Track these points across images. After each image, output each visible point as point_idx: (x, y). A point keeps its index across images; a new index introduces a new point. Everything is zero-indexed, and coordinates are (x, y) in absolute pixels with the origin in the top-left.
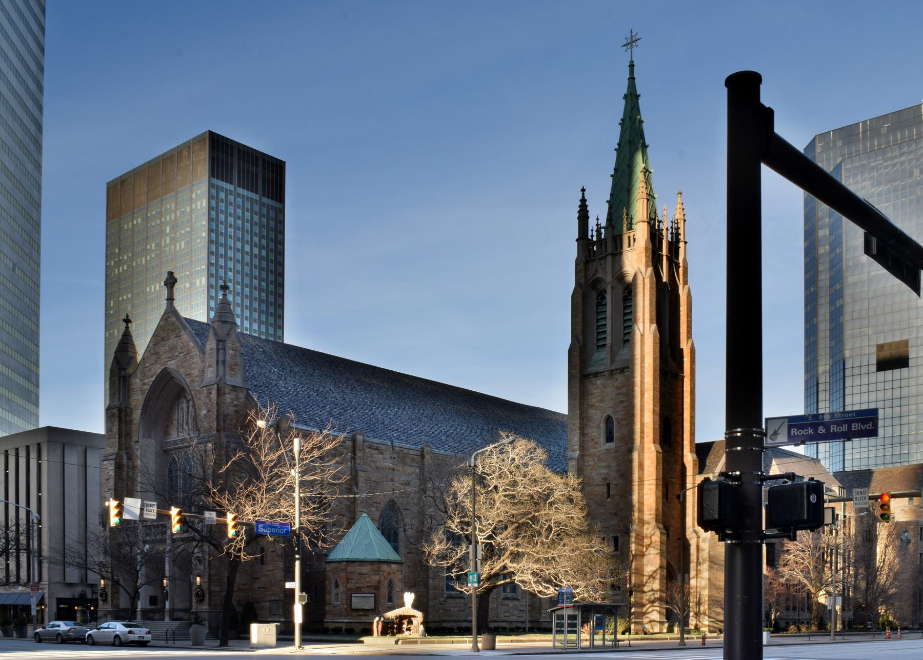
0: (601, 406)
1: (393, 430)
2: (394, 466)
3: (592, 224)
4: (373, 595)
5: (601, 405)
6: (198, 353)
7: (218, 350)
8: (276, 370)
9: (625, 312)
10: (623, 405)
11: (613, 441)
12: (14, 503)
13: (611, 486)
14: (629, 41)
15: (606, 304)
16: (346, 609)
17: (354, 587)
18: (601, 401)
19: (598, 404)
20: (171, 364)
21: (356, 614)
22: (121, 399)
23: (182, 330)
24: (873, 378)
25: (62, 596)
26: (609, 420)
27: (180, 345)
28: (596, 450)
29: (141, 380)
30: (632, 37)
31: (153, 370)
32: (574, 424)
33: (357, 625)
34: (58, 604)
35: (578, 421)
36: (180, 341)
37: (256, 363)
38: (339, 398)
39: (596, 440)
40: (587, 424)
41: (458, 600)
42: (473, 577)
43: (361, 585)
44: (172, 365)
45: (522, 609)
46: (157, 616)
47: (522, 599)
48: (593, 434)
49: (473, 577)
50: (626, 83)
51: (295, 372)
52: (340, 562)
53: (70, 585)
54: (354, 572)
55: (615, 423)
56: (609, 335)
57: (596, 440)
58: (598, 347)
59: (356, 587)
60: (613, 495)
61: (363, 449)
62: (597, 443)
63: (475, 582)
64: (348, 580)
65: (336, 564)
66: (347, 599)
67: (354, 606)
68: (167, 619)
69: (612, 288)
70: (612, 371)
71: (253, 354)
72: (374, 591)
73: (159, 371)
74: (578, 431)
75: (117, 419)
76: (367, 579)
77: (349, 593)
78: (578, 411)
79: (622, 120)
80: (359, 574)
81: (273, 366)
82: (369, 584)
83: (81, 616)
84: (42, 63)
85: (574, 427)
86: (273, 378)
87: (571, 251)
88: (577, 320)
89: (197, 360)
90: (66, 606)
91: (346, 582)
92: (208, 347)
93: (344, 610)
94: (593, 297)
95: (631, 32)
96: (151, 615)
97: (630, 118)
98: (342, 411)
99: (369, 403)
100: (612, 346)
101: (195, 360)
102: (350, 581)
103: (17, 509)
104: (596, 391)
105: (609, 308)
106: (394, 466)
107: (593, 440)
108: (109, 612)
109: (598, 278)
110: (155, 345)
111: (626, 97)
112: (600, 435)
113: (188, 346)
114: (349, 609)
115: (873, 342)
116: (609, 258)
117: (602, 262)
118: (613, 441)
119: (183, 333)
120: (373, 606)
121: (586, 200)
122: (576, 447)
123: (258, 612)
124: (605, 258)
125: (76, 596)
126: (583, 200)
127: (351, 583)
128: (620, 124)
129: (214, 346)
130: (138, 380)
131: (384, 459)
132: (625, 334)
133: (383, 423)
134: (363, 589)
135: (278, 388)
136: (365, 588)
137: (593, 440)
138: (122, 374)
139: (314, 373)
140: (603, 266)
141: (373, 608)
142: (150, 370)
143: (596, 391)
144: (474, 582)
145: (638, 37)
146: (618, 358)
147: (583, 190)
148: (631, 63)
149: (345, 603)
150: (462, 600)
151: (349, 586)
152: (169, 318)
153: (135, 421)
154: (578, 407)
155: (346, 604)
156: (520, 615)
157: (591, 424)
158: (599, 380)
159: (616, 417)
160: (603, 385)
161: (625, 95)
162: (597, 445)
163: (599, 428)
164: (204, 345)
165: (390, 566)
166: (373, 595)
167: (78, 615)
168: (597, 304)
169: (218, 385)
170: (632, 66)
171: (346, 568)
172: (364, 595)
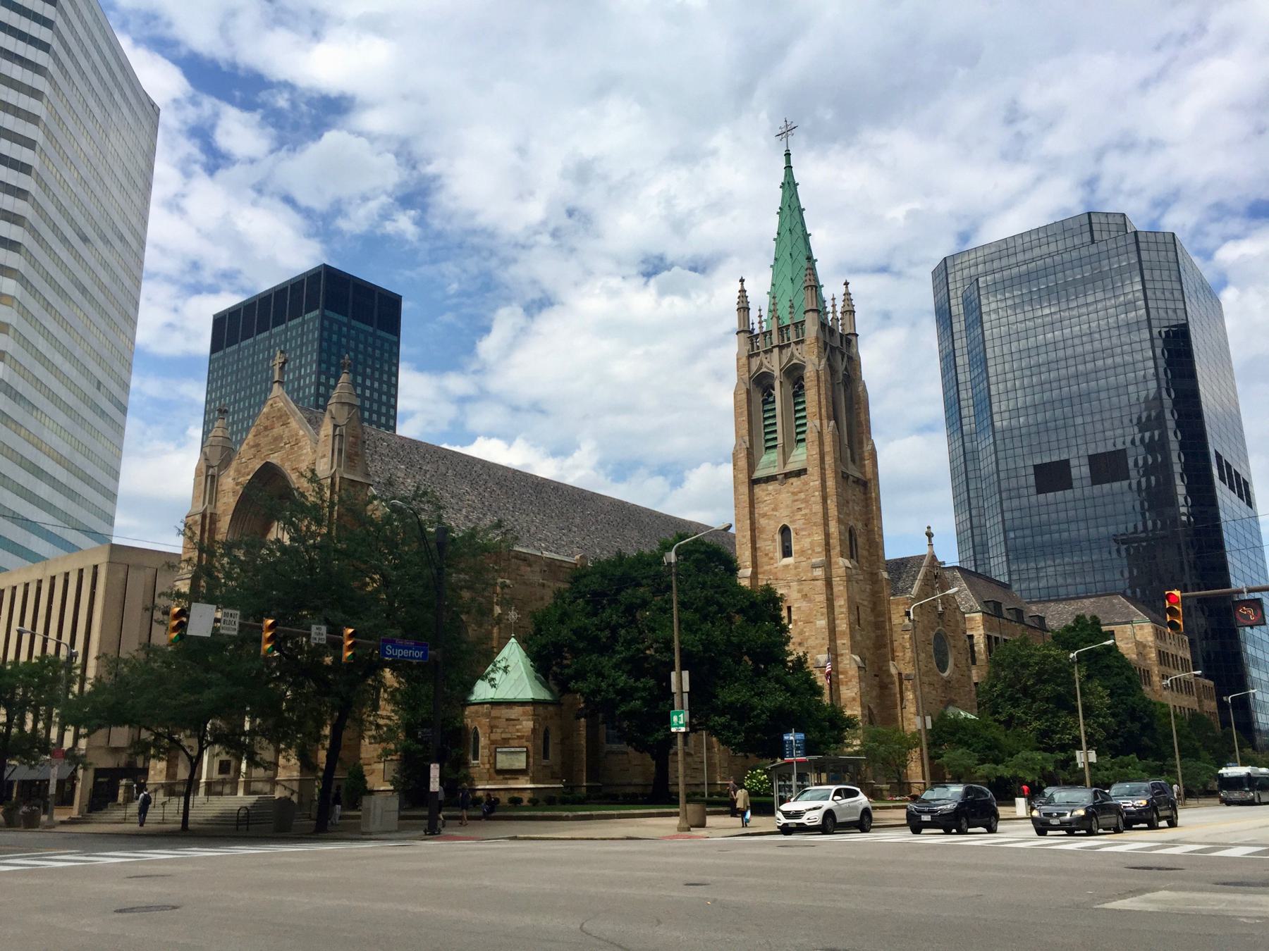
1: (540, 540)
2: (545, 582)
3: (754, 316)
4: (525, 749)
5: (775, 513)
6: (309, 442)
7: (334, 436)
8: (402, 467)
9: (797, 408)
12: (55, 638)
13: (792, 609)
14: (784, 130)
16: (488, 769)
18: (773, 510)
20: (273, 458)
21: (501, 777)
24: (1033, 499)
25: (102, 765)
26: (785, 531)
27: (287, 434)
28: (772, 567)
29: (234, 479)
30: (787, 126)
32: (744, 537)
33: (502, 793)
34: (96, 778)
35: (749, 532)
39: (771, 555)
42: (679, 718)
43: (509, 736)
44: (275, 459)
45: (695, 767)
46: (227, 789)
47: (695, 754)
48: (767, 548)
49: (679, 718)
52: (482, 703)
53: (116, 750)
54: (500, 718)
55: (793, 534)
57: (771, 555)
58: (768, 448)
59: (503, 739)
60: (795, 621)
61: (509, 560)
62: (772, 559)
63: (682, 725)
64: (492, 727)
65: (476, 707)
66: (491, 755)
67: (499, 766)
68: (241, 793)
69: (781, 382)
72: (526, 744)
73: (258, 467)
74: (750, 545)
75: (199, 527)
76: (517, 727)
77: (495, 746)
78: (748, 522)
79: (780, 208)
80: (507, 720)
82: (519, 734)
83: (125, 793)
84: (1243, 475)
85: (745, 540)
86: (398, 475)
87: (730, 352)
89: (308, 450)
90: (106, 780)
91: (489, 731)
92: (322, 433)
96: (219, 788)
98: (481, 516)
101: (305, 451)
102: (494, 730)
103: (45, 641)
106: (545, 582)
107: (767, 555)
108: (162, 786)
109: (763, 372)
110: (254, 436)
113: (297, 435)
115: (1029, 463)
116: (776, 350)
117: (768, 356)
118: (791, 555)
119: (291, 420)
120: (525, 764)
122: (748, 563)
123: (367, 778)
124: (771, 351)
125: (122, 765)
126: (743, 291)
127: (496, 732)
129: (330, 431)
130: (230, 480)
131: (532, 571)
132: (798, 434)
134: (510, 741)
135: (406, 487)
136: (515, 739)
137: (767, 555)
138: (210, 473)
140: (768, 359)
141: (525, 768)
143: (768, 498)
144: (680, 725)
145: (793, 126)
146: (791, 459)
147: (742, 281)
151: (493, 737)
153: (222, 530)
155: (489, 762)
156: (694, 775)
157: (764, 536)
160: (776, 490)
161: (783, 184)
162: (772, 561)
163: (774, 541)
164: (318, 434)
166: (525, 749)
167: (120, 791)
169: (332, 479)
170: (788, 155)
172: (513, 750)
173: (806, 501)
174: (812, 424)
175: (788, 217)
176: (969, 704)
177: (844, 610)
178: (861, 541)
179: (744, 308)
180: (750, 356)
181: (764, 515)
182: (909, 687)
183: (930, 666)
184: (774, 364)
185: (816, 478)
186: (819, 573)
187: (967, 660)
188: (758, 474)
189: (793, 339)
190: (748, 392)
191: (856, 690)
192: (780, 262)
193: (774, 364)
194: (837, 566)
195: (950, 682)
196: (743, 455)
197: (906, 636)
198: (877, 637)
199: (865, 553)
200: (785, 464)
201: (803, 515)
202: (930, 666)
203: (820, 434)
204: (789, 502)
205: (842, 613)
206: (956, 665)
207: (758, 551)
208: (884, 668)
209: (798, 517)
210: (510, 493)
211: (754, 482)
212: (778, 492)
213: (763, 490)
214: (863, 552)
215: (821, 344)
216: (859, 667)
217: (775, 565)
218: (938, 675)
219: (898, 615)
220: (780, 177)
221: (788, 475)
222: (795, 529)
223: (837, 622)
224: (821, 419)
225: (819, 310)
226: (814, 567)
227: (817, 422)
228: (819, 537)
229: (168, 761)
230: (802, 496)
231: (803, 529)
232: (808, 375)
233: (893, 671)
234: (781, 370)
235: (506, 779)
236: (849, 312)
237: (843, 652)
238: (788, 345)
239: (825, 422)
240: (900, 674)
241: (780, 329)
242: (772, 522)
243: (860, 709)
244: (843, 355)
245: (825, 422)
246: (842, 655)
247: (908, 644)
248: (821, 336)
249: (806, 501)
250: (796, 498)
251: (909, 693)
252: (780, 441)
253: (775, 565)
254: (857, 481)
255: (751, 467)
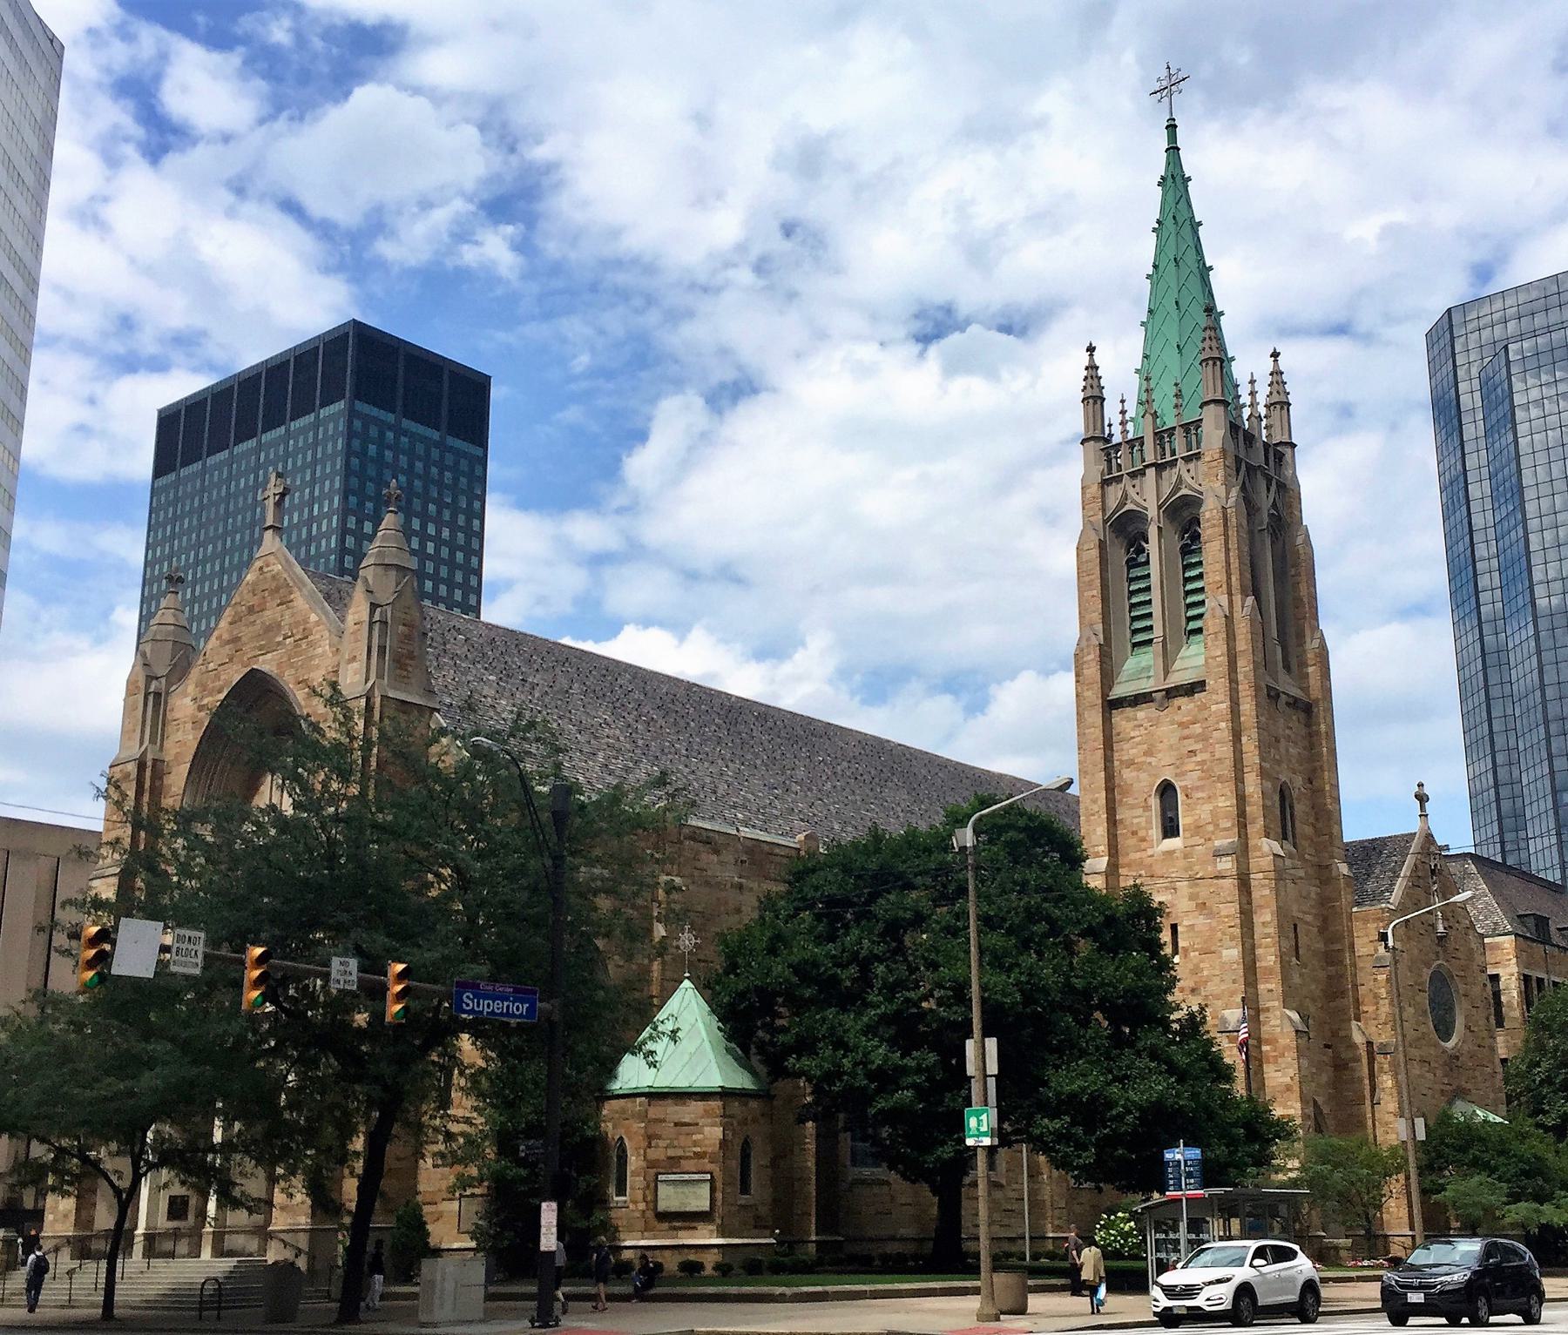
0: (1150, 763)
1: (735, 807)
3: (1111, 412)
4: (708, 1177)
6: (326, 634)
8: (491, 678)
9: (1187, 575)
10: (1194, 759)
11: (1178, 835)
14: (1165, 83)
15: (1147, 563)
17: (663, 1157)
18: (1148, 753)
19: (1143, 759)
21: (665, 1226)
22: (146, 742)
23: (296, 589)
26: (1167, 791)
28: (1143, 854)
31: (222, 677)
32: (1095, 801)
33: (667, 1253)
36: (288, 612)
37: (452, 663)
38: (622, 738)
39: (1142, 833)
40: (1121, 801)
41: (876, 1190)
42: (979, 1121)
43: (680, 1153)
44: (266, 664)
47: (1009, 1184)
48: (1135, 821)
50: (1163, 157)
51: (531, 683)
55: (1181, 797)
56: (1157, 622)
57: (1142, 833)
58: (1135, 645)
62: (1143, 840)
63: (985, 1134)
64: (650, 1138)
65: (622, 1101)
66: (648, 1187)
67: (663, 1206)
68: (206, 1253)
70: (1168, 691)
71: (445, 644)
78: (1102, 774)
79: (1158, 222)
80: (676, 1124)
81: (486, 669)
82: (698, 1149)
88: (1090, 593)
89: (324, 648)
93: (638, 1214)
94: (1119, 556)
95: (1168, 68)
96: (168, 1246)
97: (1174, 217)
98: (631, 765)
99: (684, 752)
100: (1164, 642)
101: (320, 650)
104: (1137, 733)
105: (1154, 569)
110: (231, 624)
111: (1163, 182)
112: (1149, 822)
113: (306, 621)
114: (650, 1214)
116: (1151, 472)
117: (1137, 482)
118: (1178, 835)
121: (1097, 368)
122: (1102, 848)
123: (429, 1227)
124: (1142, 473)
126: (1092, 367)
127: (657, 1146)
128: (1154, 230)
130: (188, 701)
133: (715, 792)
136: (687, 1158)
137: (1134, 833)
139: (571, 688)
140: (1138, 489)
142: (218, 677)
143: (1137, 733)
146: (1178, 665)
147: (1091, 349)
148: (1171, 122)
149: (640, 1197)
150: (885, 1188)
151: (654, 1154)
152: (268, 566)
154: (1103, 765)
156: (1006, 1221)
158: (1141, 710)
159: (1183, 784)
162: (1144, 845)
163: (1147, 808)
165: (746, 1104)
166: (708, 1177)
168: (1127, 562)
170: (1172, 128)
171: (646, 1111)
172: (686, 1177)
173: (1203, 738)
174: (1215, 602)
175: (1173, 237)
176: (1492, 1096)
177: (1271, 930)
178: (1300, 808)
179: (1094, 398)
180: (1105, 483)
181: (1130, 763)
182: (1386, 1066)
183: (1423, 1029)
184: (1148, 496)
185: (1221, 697)
186: (1227, 865)
187: (1488, 1019)
188: (1118, 691)
189: (1181, 452)
190: (1102, 545)
191: (1292, 1072)
192: (1159, 317)
193: (1148, 496)
194: (1258, 854)
195: (1457, 1058)
196: (1092, 656)
197: (1379, 977)
198: (1329, 977)
199: (1308, 830)
200: (1166, 673)
201: (1198, 763)
202: (1423, 1029)
203: (1229, 619)
204: (1174, 740)
205: (1267, 936)
206: (1468, 1028)
207: (1120, 827)
208: (1342, 1033)
209: (1191, 767)
210: (682, 723)
211: (1112, 705)
212: (1156, 723)
213: (1128, 720)
214: (1304, 829)
215: (1230, 461)
216: (1297, 1031)
217: (1150, 852)
218: (1436, 1045)
219: (1366, 940)
220: (1159, 167)
221: (1171, 693)
222: (1185, 788)
223: (1259, 951)
224: (1230, 594)
225: (1227, 401)
226: (1218, 854)
227: (1224, 600)
228: (1227, 803)
229: (78, 1197)
230: (1197, 728)
231: (1197, 788)
232: (1208, 515)
233: (1358, 1038)
234: (1159, 507)
235: (675, 1229)
236: (1281, 404)
237: (1269, 1004)
238: (1173, 463)
239: (1237, 598)
240: (1369, 1044)
241: (1158, 435)
242: (1143, 776)
243: (1298, 1105)
244: (1269, 480)
245: (1237, 598)
246: (1268, 1010)
247: (1383, 991)
248: (1231, 447)
249: (1203, 738)
250: (1186, 732)
251: (1385, 1077)
252: (1158, 632)
253: (1150, 852)
254: (1294, 703)
255: (1108, 677)
